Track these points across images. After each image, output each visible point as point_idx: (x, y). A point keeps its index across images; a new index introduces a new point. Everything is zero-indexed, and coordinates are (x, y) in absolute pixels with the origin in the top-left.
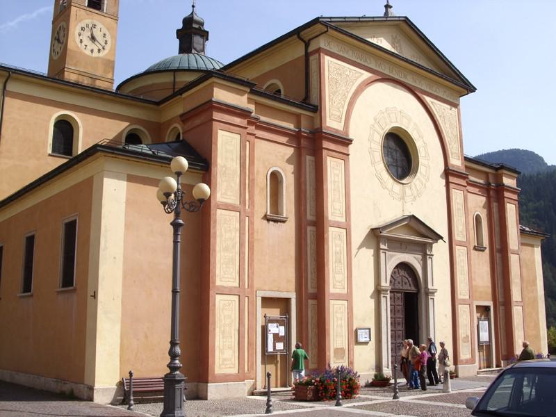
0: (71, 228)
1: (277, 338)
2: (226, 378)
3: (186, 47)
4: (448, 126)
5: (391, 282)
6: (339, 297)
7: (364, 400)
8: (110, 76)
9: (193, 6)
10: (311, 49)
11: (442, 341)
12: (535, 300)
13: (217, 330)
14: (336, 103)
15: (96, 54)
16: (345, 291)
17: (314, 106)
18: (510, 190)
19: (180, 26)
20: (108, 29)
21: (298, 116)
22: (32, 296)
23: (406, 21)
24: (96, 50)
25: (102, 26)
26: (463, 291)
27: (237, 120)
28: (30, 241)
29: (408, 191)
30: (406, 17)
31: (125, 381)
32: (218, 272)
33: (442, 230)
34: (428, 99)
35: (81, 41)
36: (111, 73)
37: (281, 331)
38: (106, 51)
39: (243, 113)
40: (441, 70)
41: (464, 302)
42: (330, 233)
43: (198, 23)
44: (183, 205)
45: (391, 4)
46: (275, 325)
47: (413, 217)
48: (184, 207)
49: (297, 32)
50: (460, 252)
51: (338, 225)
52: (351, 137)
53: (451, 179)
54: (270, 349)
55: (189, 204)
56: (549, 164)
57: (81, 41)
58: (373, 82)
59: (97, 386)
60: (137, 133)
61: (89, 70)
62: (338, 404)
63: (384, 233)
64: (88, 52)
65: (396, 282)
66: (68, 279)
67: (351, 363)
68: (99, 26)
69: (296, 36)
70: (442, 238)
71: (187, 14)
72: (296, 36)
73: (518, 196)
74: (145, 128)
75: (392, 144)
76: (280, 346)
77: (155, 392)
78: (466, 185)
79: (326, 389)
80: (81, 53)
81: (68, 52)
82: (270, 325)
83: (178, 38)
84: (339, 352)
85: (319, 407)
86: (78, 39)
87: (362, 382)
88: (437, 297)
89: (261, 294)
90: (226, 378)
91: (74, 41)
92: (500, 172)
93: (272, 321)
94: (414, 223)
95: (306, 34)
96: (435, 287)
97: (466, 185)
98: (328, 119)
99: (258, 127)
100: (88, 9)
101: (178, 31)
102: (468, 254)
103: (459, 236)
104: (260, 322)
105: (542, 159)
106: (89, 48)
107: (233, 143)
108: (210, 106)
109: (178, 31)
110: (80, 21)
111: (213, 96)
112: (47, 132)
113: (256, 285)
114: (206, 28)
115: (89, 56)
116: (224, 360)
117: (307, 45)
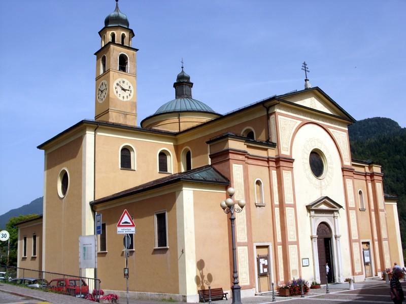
1: (264, 266)
2: (246, 288)
3: (179, 95)
4: (342, 143)
6: (293, 243)
7: (313, 295)
8: (134, 112)
9: (182, 68)
10: (269, 113)
11: (127, 172)
12: (395, 236)
13: (239, 264)
15: (125, 99)
16: (295, 240)
17: (274, 143)
18: (378, 175)
20: (131, 83)
22: (84, 245)
23: (317, 89)
24: (125, 97)
25: (128, 82)
26: (355, 236)
27: (241, 157)
29: (323, 184)
30: (317, 87)
31: (387, 273)
32: (237, 235)
33: (342, 203)
34: (331, 130)
35: (117, 92)
36: (135, 111)
37: (266, 262)
38: (131, 97)
39: (243, 153)
40: (337, 113)
41: (356, 241)
42: (286, 210)
45: (308, 79)
46: (263, 259)
47: (327, 198)
49: (263, 103)
50: (353, 214)
51: (290, 206)
52: (293, 158)
53: (346, 173)
54: (262, 272)
56: (402, 127)
57: (117, 92)
58: (303, 125)
59: (188, 294)
60: (165, 153)
61: (123, 109)
62: (302, 297)
63: (313, 208)
64: (121, 98)
67: (300, 277)
68: (126, 81)
70: (342, 207)
71: (179, 72)
73: (382, 178)
74: (168, 149)
76: (266, 270)
79: (294, 290)
80: (118, 99)
81: (110, 100)
82: (260, 260)
84: (295, 271)
85: (294, 298)
86: (116, 93)
87: (309, 286)
88: (341, 239)
89: (255, 245)
90: (246, 288)
91: (113, 91)
92: (371, 165)
93: (261, 258)
94: (326, 200)
95: (267, 104)
96: (340, 234)
98: (282, 150)
99: (248, 158)
100: (119, 72)
102: (357, 213)
103: (352, 204)
104: (255, 257)
105: (396, 123)
106: (122, 96)
108: (227, 152)
110: (116, 79)
112: (118, 156)
113: (254, 240)
114: (191, 81)
115: (121, 101)
116: (243, 279)
117: (268, 110)
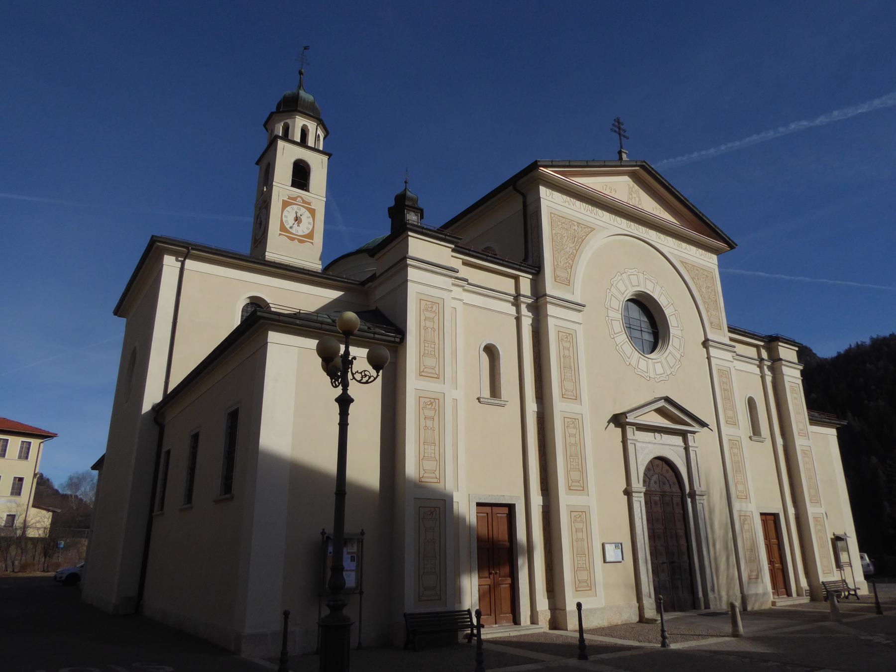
0: (234, 416)
5: (644, 481)
9: (406, 182)
14: (562, 263)
16: (271, 254)
19: (392, 204)
21: (516, 278)
28: (195, 438)
43: (411, 199)
44: (353, 374)
47: (667, 400)
48: (354, 378)
55: (361, 373)
65: (652, 482)
66: (227, 486)
69: (511, 188)
71: (399, 191)
72: (511, 188)
75: (635, 312)
77: (846, 563)
78: (732, 360)
83: (390, 217)
97: (732, 360)
101: (390, 209)
107: (434, 309)
109: (390, 209)
111: (408, 254)
